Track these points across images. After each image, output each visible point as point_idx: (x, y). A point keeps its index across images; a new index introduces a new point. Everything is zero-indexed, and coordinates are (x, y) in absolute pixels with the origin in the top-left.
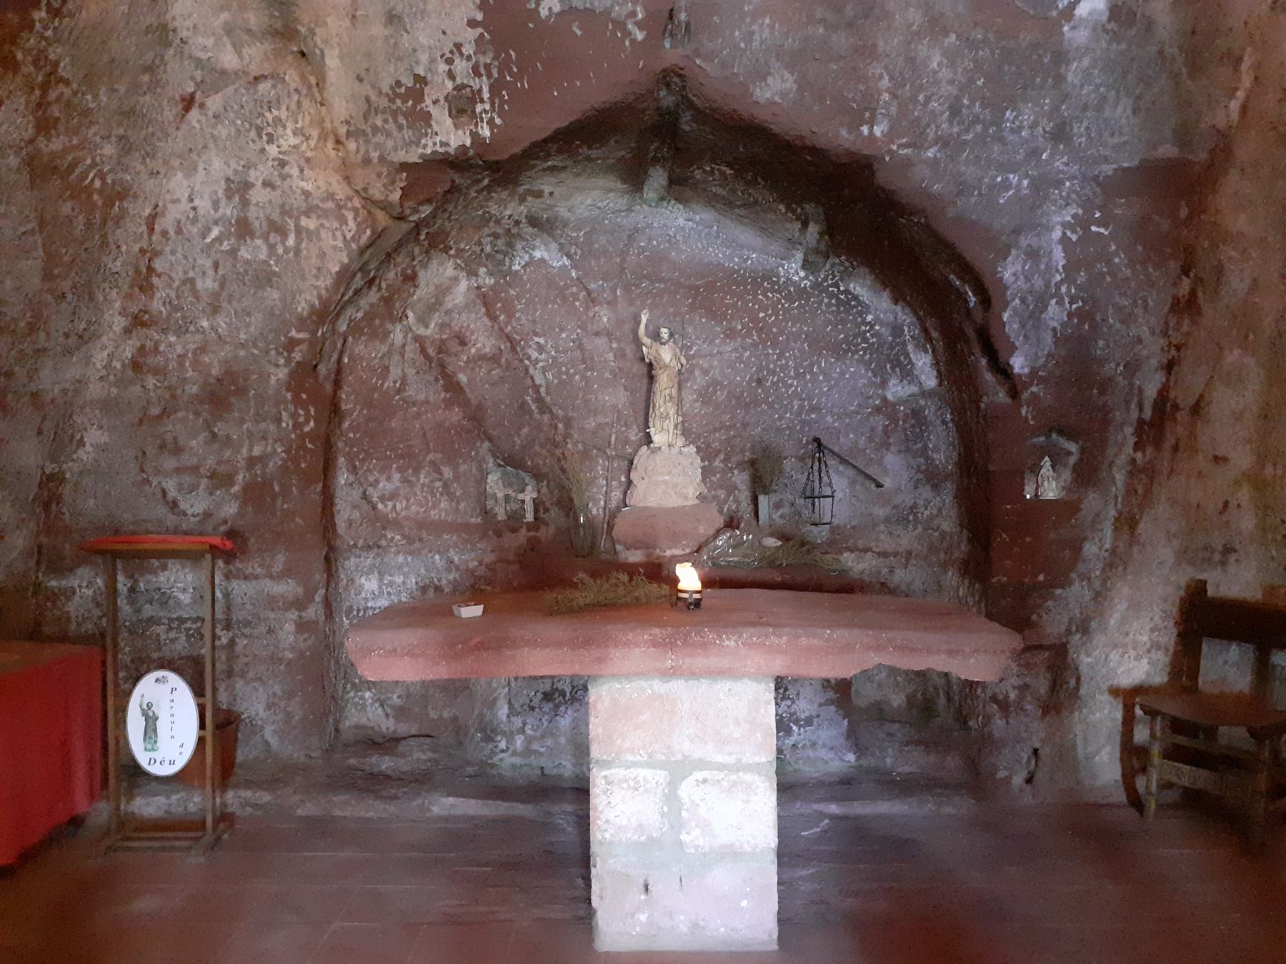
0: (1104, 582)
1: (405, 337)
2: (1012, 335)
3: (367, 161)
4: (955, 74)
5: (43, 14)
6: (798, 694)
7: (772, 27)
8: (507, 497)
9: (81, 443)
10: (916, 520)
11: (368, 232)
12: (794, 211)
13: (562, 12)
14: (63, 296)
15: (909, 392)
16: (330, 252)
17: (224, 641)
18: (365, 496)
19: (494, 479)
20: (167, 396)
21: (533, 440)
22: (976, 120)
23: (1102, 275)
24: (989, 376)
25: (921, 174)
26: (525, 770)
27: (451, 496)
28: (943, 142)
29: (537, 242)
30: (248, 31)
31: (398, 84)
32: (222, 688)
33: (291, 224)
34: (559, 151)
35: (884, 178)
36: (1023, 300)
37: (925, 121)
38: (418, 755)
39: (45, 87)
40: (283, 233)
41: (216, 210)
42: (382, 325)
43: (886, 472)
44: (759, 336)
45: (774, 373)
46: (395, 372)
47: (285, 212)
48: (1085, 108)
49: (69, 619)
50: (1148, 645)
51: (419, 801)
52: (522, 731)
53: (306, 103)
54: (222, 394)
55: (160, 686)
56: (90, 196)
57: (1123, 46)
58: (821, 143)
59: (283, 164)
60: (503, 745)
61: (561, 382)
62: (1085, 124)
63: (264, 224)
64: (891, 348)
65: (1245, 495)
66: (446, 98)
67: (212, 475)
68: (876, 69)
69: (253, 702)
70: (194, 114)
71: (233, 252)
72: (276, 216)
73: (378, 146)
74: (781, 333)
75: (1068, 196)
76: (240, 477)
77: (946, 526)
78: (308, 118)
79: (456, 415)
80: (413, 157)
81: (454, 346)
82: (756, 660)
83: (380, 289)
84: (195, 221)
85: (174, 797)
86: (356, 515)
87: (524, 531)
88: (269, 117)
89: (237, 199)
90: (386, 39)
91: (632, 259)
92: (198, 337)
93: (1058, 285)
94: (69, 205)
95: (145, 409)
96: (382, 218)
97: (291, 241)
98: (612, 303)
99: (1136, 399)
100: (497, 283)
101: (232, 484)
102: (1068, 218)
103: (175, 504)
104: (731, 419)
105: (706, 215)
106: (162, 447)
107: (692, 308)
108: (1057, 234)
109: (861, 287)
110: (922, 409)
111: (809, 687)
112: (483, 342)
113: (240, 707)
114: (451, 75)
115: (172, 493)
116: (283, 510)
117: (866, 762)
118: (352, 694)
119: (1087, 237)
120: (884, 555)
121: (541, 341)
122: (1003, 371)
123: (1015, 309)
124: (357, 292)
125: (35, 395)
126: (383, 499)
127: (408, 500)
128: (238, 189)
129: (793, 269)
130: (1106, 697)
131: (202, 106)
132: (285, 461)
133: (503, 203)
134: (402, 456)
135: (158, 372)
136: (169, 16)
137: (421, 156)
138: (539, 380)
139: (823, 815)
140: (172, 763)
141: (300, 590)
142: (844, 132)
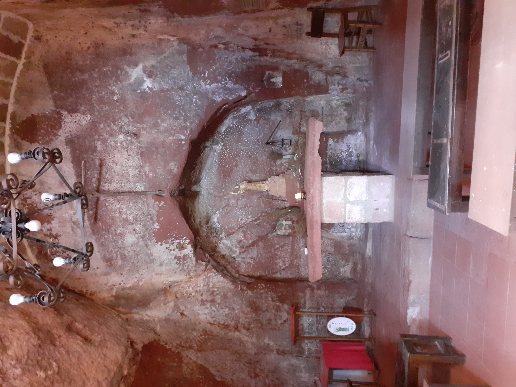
0: (307, 60)
3: (196, 270)
8: (285, 229)
9: (268, 344)
10: (291, 109)
14: (231, 346)
17: (323, 309)
18: (284, 270)
23: (219, 72)
24: (247, 99)
26: (361, 228)
27: (284, 245)
28: (185, 121)
30: (165, 299)
31: (176, 263)
32: (336, 311)
33: (211, 289)
34: (190, 219)
35: (195, 136)
40: (213, 292)
43: (276, 119)
45: (248, 153)
46: (249, 260)
47: (208, 291)
48: (175, 82)
52: (350, 229)
53: (182, 286)
54: (255, 308)
57: (158, 73)
58: (187, 154)
59: (197, 291)
60: (354, 234)
61: (251, 214)
62: (179, 82)
65: (280, 21)
68: (168, 141)
70: (185, 313)
71: (219, 304)
72: (210, 293)
73: (192, 268)
74: (236, 151)
76: (277, 304)
79: (261, 244)
80: (194, 259)
81: (242, 244)
82: (317, 184)
85: (365, 324)
86: (289, 272)
87: (294, 225)
90: (166, 266)
91: (216, 194)
92: (241, 314)
96: (209, 266)
97: (216, 289)
103: (285, 321)
105: (204, 174)
106: (269, 324)
107: (230, 176)
108: (208, 86)
109: (223, 129)
110: (258, 109)
112: (240, 236)
114: (174, 250)
115: (282, 321)
119: (209, 78)
120: (301, 119)
121: (240, 219)
122: (246, 97)
124: (228, 272)
125: (256, 354)
126: (285, 265)
129: (218, 148)
131: (183, 311)
133: (203, 232)
135: (249, 324)
137: (194, 257)
138: (251, 220)
139: (373, 146)
141: (308, 289)
142: (184, 148)
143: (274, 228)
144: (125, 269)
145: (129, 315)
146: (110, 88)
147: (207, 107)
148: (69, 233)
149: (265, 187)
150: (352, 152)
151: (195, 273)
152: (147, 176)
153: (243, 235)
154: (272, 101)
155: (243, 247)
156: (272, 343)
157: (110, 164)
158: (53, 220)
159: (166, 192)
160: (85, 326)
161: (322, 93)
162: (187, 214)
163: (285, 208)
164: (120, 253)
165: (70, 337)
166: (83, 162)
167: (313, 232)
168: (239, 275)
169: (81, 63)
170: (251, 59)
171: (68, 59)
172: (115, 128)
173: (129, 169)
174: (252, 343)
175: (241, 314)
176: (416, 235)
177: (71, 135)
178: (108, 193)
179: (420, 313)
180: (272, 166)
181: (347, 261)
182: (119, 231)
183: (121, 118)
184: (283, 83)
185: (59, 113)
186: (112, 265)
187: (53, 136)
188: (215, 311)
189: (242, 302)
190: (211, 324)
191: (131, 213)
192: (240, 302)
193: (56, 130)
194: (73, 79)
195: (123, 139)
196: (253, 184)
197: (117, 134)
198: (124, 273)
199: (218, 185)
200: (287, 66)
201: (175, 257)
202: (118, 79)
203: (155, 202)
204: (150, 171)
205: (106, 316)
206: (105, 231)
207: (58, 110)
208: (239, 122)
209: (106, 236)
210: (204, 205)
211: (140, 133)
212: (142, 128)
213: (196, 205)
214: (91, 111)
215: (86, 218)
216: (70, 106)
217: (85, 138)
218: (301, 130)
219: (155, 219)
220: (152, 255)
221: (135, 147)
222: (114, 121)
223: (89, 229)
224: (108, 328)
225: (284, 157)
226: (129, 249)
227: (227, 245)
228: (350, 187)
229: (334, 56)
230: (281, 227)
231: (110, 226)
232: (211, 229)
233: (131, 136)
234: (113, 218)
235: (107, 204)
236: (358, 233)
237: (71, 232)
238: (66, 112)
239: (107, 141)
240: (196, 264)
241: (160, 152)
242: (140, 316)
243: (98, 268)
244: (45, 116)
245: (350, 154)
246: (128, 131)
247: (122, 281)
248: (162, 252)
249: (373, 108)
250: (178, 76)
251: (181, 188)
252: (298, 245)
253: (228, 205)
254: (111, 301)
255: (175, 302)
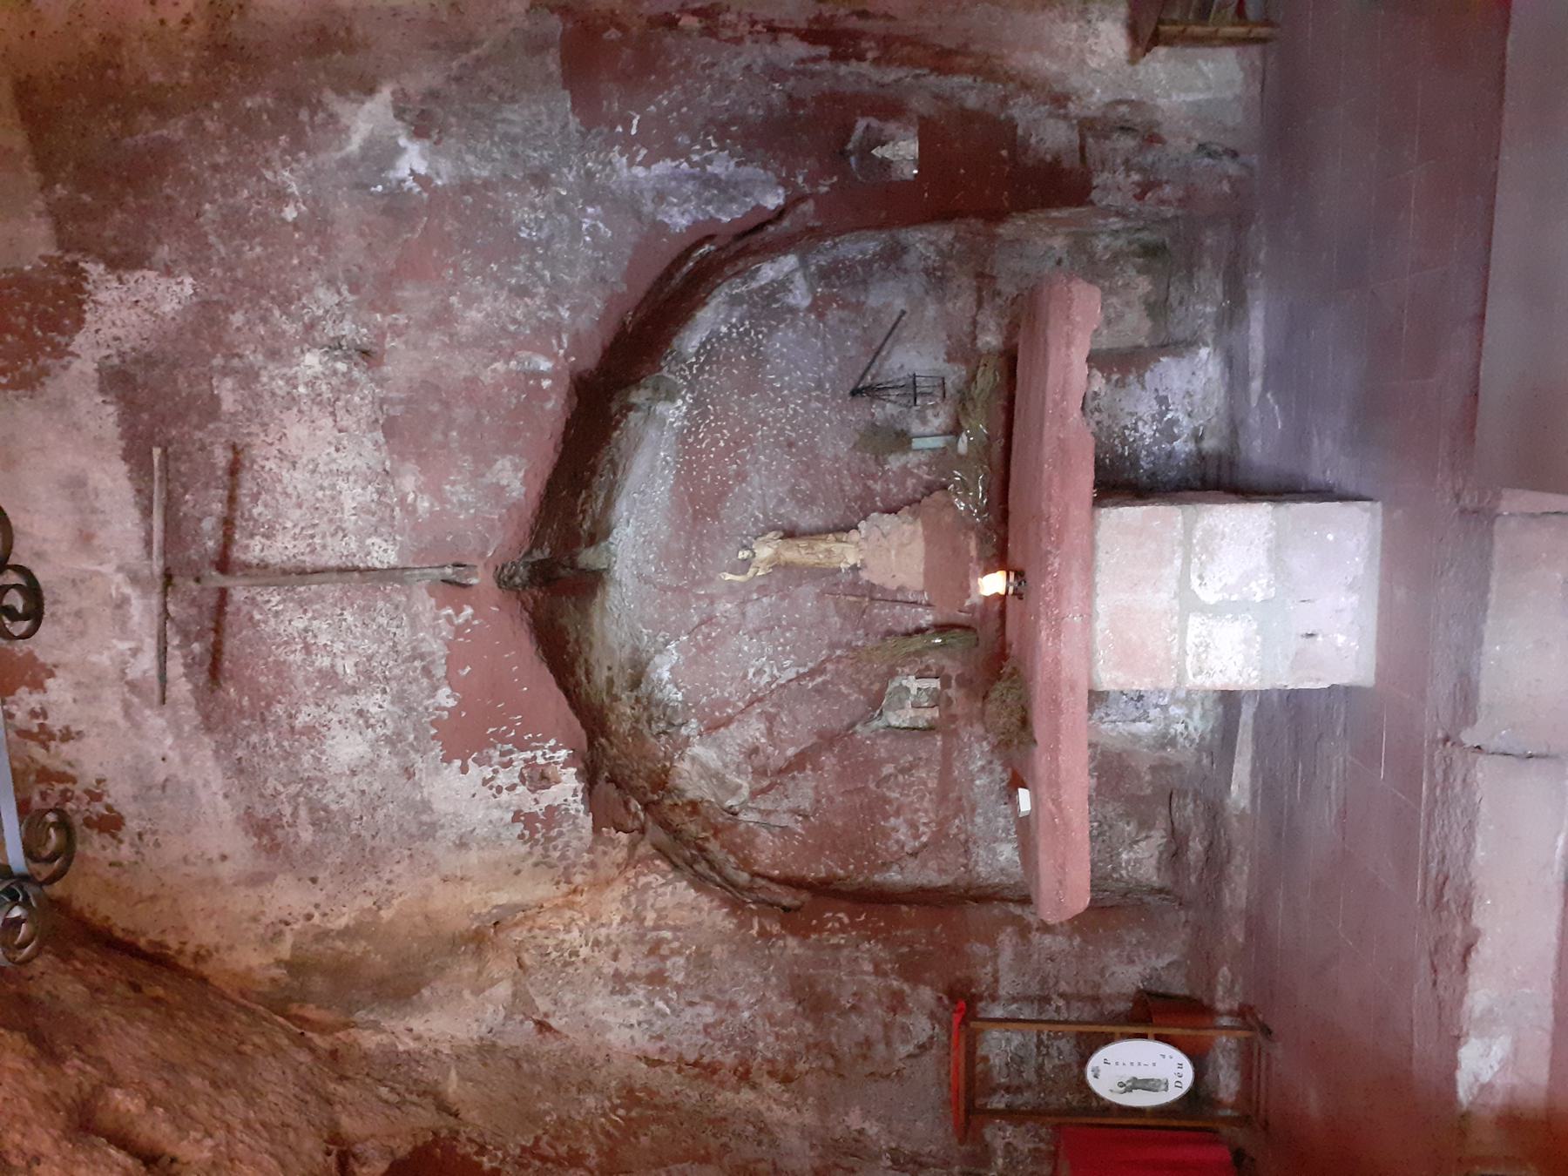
0: (1011, 79)
1: (752, 809)
2: (744, 210)
3: (593, 865)
4: (487, 294)
5: (485, 1159)
6: (1132, 414)
7: (453, 484)
8: (916, 706)
9: (861, 1132)
11: (658, 862)
12: (619, 422)
13: (450, 685)
14: (724, 1145)
15: (802, 281)
16: (676, 899)
18: (914, 854)
19: (894, 719)
20: (815, 1051)
21: (854, 681)
22: (531, 269)
24: (786, 223)
25: (585, 321)
28: (553, 302)
29: (654, 676)
30: (480, 973)
31: (521, 836)
33: (651, 935)
34: (573, 674)
35: (590, 360)
36: (709, 202)
37: (534, 322)
38: (1189, 811)
39: (544, 1159)
40: (659, 943)
41: (639, 1004)
42: (741, 836)
43: (888, 305)
44: (744, 446)
45: (782, 430)
46: (786, 820)
47: (640, 939)
48: (514, 155)
49: (1036, 1149)
50: (1082, 23)
51: (1234, 820)
52: (1165, 708)
53: (541, 921)
54: (814, 1001)
55: (1101, 1075)
56: (631, 1119)
58: (561, 426)
59: (597, 943)
60: (1180, 727)
61: (793, 651)
63: (652, 958)
64: (754, 305)
66: (533, 792)
67: (894, 1010)
68: (487, 377)
69: (1126, 975)
70: (553, 1022)
71: (678, 988)
72: (645, 949)
73: (578, 855)
74: (740, 423)
75: (602, 163)
76: (895, 983)
77: (948, 235)
78: (554, 920)
79: (828, 760)
81: (759, 760)
83: (706, 839)
84: (651, 1024)
85: (1221, 1061)
86: (932, 864)
88: (554, 955)
89: (630, 985)
91: (667, 580)
92: (759, 1021)
93: (692, 164)
94: (643, 1139)
95: (828, 1072)
96: (644, 849)
97: (668, 934)
98: (712, 600)
99: (811, 66)
100: (695, 716)
101: (902, 992)
102: (624, 160)
104: (831, 473)
105: (622, 507)
107: (716, 516)
108: (640, 171)
109: (691, 341)
110: (820, 268)
111: (1123, 403)
113: (1130, 989)
114: (512, 788)
115: (910, 1048)
116: (927, 944)
117: (1208, 332)
118: (1124, 872)
119: (643, 138)
120: (980, 305)
121: (751, 671)
122: (780, 213)
123: (718, 210)
124: (711, 865)
127: (917, 810)
128: (620, 983)
129: (674, 412)
130: (1140, 67)
131: (546, 1015)
132: (877, 942)
134: (873, 815)
135: (791, 1061)
136: (470, 1044)
137: (586, 813)
138: (791, 674)
139: (1262, 396)
140: (1180, 1066)
141: (1009, 929)
142: (549, 405)
143: (876, 703)
144: (328, 861)
145: (340, 1035)
146: (269, 175)
147: (637, 248)
148: (113, 724)
149: (846, 553)
150: (1174, 422)
151: (590, 872)
152: (410, 511)
153: (762, 726)
154: (873, 239)
155: (764, 774)
156: (875, 1129)
157: (268, 465)
158: (51, 675)
159: (480, 570)
160: (150, 1104)
161: (1067, 203)
162: (560, 651)
163: (920, 631)
164: (309, 800)
165: (81, 1157)
166: (157, 452)
167: (1056, 729)
168: (755, 875)
169: (157, 78)
170: (802, 70)
171: (108, 65)
172: (290, 328)
173: (341, 485)
174: (804, 1131)
175: (759, 1021)
176: (1503, 747)
177: (121, 354)
178: (264, 573)
179: (1513, 1059)
180: (873, 476)
181: (1145, 824)
182: (301, 720)
183: (309, 289)
184: (923, 161)
185: (74, 270)
186: (279, 845)
187: (49, 355)
188: (664, 1015)
189: (767, 979)
190: (652, 1063)
191: (350, 650)
192: (758, 980)
193: (62, 333)
194: (128, 141)
195: (319, 368)
196: (803, 543)
197: (297, 350)
198: (322, 875)
199: (674, 546)
200: (937, 97)
201: (517, 816)
202: (298, 142)
203: (440, 606)
204: (419, 490)
205: (248, 1048)
206: (252, 717)
207: (68, 258)
208: (752, 316)
209: (254, 738)
210: (624, 619)
211: (382, 345)
212: (390, 326)
213: (596, 620)
214: (197, 261)
215: (175, 668)
216: (115, 241)
217: (175, 365)
218: (979, 344)
219: (440, 672)
220: (426, 806)
221: (363, 397)
222: (285, 301)
223: (192, 711)
224: (249, 1103)
225: (917, 443)
226: (342, 786)
227: (705, 764)
228: (1205, 549)
229: (1110, 61)
230: (900, 700)
231: (270, 701)
232: (650, 706)
233: (347, 357)
234: (280, 669)
235: (257, 617)
236: (1195, 724)
237: (122, 723)
238: (102, 267)
239: (257, 375)
240: (594, 841)
241: (460, 420)
242: (383, 1038)
243: (224, 858)
244: (22, 280)
245: (1168, 431)
246: (338, 339)
247: (317, 906)
248: (466, 795)
249: (1262, 256)
250: (527, 130)
251: (538, 555)
252: (965, 764)
253: (709, 620)
254: (273, 980)
255: (515, 984)
